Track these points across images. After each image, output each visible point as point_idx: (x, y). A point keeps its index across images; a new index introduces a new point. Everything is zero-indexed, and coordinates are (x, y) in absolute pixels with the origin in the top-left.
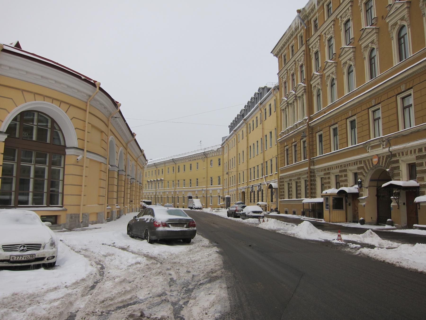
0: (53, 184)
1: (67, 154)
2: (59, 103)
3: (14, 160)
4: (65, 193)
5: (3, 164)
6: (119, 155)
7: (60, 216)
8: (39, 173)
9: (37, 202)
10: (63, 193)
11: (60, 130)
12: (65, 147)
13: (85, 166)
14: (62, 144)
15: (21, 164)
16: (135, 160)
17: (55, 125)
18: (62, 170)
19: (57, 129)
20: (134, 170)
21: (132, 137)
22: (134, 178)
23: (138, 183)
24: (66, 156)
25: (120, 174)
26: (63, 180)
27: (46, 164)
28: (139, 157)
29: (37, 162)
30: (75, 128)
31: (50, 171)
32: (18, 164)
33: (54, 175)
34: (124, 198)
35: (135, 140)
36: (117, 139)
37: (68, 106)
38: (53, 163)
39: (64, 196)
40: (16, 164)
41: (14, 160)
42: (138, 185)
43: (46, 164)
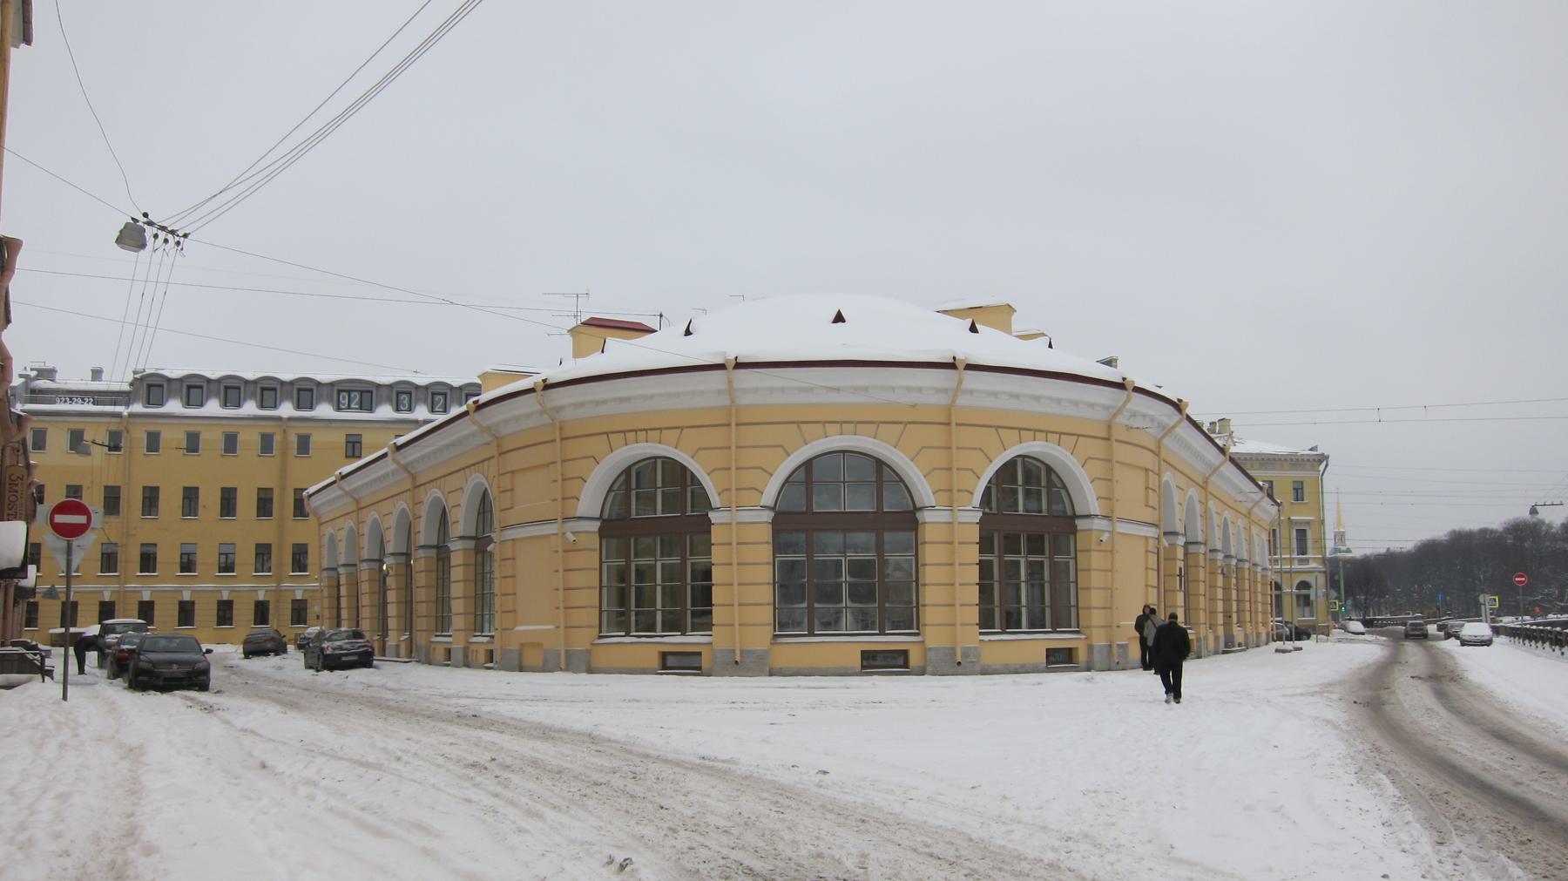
0: (622, 598)
1: (1078, 528)
2: (1044, 434)
3: (1043, 553)
4: (1080, 605)
5: (980, 560)
6: (1185, 508)
7: (1077, 648)
8: (1035, 570)
9: (1037, 623)
10: (1077, 607)
11: (1065, 487)
12: (1075, 517)
13: (561, 591)
14: (1069, 513)
15: (1006, 559)
16: (1198, 484)
17: (1054, 477)
18: (1072, 563)
19: (1059, 486)
20: (1216, 528)
21: (1176, 413)
22: (1200, 539)
23: (1259, 569)
24: (1078, 534)
25: (1191, 553)
26: (1076, 582)
27: (1069, 555)
28: (1215, 470)
29: (1030, 551)
30: (1092, 478)
31: (1053, 565)
32: (1051, 558)
33: (1060, 572)
34: (1250, 601)
35: (1189, 418)
36: (1179, 474)
37: (1058, 435)
38: (1056, 550)
39: (1080, 611)
40: (1048, 560)
41: (1043, 553)
42: (1259, 575)
43: (1069, 555)
